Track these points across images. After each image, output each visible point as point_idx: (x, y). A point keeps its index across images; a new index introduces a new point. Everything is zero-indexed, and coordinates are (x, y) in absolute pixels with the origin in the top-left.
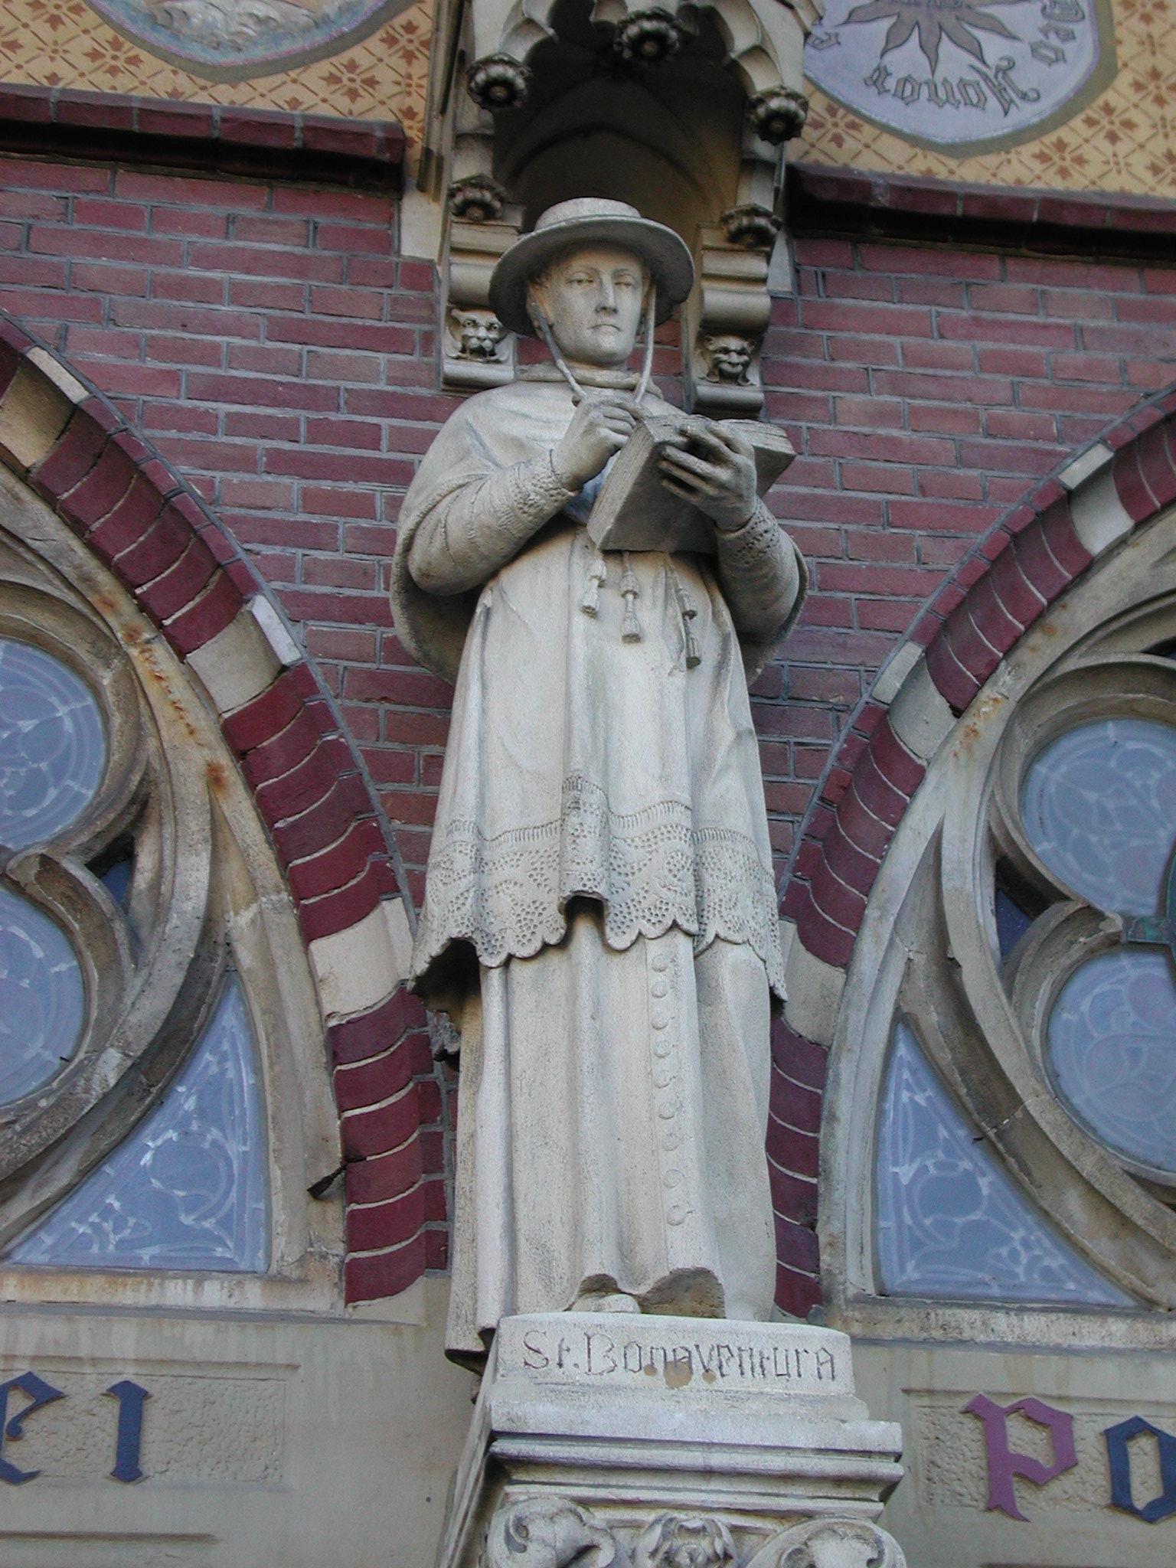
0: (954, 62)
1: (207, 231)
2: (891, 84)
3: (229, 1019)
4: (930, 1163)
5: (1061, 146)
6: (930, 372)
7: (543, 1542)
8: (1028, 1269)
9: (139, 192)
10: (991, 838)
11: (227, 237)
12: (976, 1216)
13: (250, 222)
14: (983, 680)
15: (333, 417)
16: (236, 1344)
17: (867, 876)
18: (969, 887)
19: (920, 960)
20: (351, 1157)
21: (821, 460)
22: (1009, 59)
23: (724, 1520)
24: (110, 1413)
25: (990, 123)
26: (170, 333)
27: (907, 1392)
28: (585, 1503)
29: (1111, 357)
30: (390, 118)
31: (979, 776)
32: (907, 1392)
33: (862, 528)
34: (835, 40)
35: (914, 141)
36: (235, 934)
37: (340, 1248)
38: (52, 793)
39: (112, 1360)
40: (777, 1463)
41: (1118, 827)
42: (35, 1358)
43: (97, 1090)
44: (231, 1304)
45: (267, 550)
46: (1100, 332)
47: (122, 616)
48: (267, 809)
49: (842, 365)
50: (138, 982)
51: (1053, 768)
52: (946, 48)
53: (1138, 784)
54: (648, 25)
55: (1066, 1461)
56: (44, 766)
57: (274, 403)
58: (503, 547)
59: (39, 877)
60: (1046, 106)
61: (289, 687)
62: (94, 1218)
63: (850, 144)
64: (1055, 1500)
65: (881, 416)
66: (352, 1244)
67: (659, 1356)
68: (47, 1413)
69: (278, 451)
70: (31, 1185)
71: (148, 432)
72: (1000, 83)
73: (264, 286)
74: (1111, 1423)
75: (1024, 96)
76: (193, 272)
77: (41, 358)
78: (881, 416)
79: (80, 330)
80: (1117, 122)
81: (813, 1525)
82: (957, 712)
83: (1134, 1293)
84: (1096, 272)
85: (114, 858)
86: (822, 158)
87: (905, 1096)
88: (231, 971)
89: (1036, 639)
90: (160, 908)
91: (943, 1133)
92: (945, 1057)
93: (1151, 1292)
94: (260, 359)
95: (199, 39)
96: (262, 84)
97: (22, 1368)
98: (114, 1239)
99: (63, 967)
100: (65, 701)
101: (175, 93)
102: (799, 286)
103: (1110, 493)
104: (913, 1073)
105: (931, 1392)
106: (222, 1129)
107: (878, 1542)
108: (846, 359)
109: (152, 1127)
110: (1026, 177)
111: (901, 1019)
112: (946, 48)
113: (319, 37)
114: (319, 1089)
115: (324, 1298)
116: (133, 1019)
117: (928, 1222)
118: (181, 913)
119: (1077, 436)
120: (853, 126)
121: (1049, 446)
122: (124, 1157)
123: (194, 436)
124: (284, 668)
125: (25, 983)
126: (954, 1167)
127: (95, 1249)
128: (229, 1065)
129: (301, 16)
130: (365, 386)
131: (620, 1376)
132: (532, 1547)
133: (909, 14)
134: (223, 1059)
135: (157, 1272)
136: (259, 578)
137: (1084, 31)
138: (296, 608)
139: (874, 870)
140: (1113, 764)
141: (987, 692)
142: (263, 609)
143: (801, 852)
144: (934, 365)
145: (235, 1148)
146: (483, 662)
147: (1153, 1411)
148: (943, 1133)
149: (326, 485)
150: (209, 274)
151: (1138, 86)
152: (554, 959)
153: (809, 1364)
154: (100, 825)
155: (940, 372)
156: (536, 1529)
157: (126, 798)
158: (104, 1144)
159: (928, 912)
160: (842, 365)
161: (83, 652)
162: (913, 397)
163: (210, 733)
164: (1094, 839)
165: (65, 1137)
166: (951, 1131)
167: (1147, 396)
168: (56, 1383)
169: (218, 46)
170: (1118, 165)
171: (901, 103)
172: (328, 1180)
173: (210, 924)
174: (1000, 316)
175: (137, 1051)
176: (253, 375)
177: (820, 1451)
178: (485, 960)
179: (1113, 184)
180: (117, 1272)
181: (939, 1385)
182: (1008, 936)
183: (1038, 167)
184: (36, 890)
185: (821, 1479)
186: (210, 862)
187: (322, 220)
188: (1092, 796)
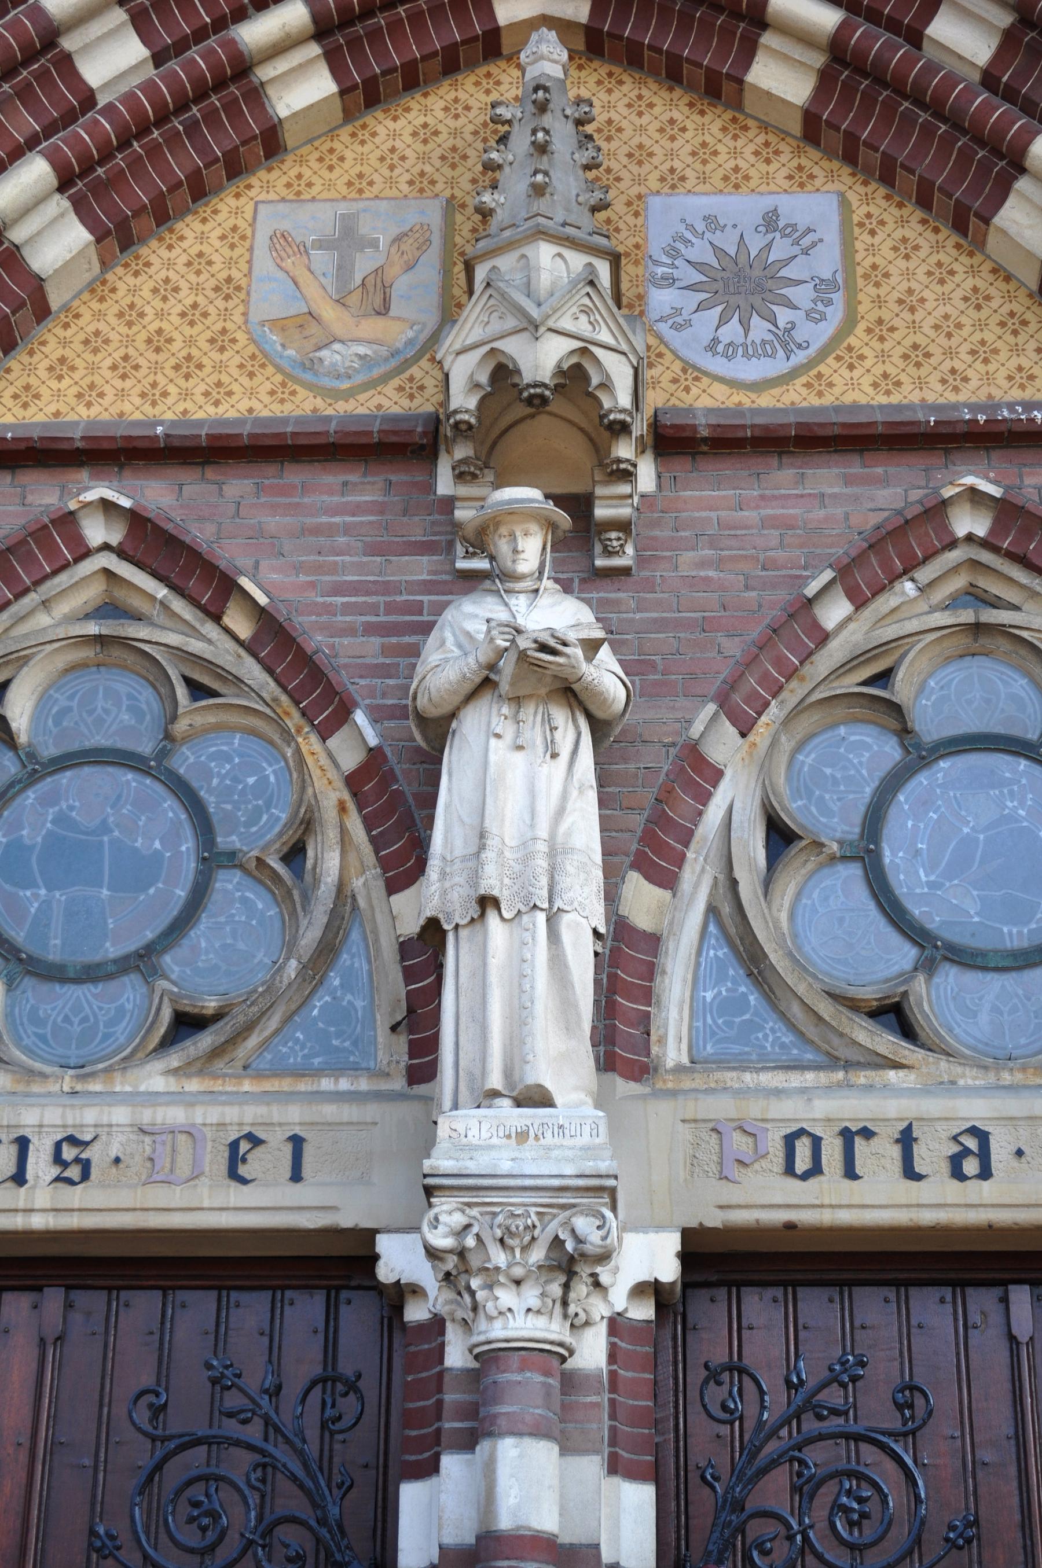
0: (759, 328)
1: (331, 493)
2: (720, 348)
3: (355, 935)
4: (723, 989)
5: (819, 376)
6: (732, 532)
7: (446, 1224)
8: (772, 1046)
9: (295, 475)
10: (764, 805)
11: (343, 495)
12: (747, 1017)
13: (355, 484)
14: (760, 714)
15: (398, 598)
16: (348, 1112)
17: (686, 837)
18: (746, 836)
19: (721, 877)
20: (411, 1011)
21: (666, 595)
22: (792, 323)
23: (533, 1210)
24: (288, 1149)
25: (777, 366)
26: (312, 558)
27: (683, 1121)
28: (469, 1205)
29: (839, 511)
30: (432, 409)
31: (755, 770)
32: (683, 1121)
33: (688, 636)
34: (689, 323)
35: (734, 384)
36: (356, 890)
37: (406, 1058)
38: (265, 817)
39: (289, 1124)
40: (556, 1182)
41: (842, 788)
42: (253, 1124)
43: (286, 982)
44: (352, 1088)
45: (363, 682)
46: (834, 496)
47: (294, 720)
48: (369, 824)
49: (683, 534)
50: (306, 922)
51: (807, 756)
52: (755, 319)
53: (855, 761)
54: (532, 391)
55: (761, 1156)
56: (260, 802)
57: (368, 593)
58: (457, 699)
59: (257, 867)
60: (812, 351)
61: (375, 755)
62: (290, 1044)
63: (694, 391)
64: (757, 1172)
65: (703, 564)
66: (411, 1056)
67: (513, 1130)
68: (259, 1151)
69: (368, 622)
70: (257, 1031)
71: (300, 619)
72: (786, 340)
73: (362, 523)
74: (789, 1131)
75: (799, 346)
76: (324, 519)
77: (245, 582)
78: (703, 564)
79: (264, 564)
80: (884, 328)
81: (574, 1210)
82: (743, 735)
83: (828, 1054)
84: (836, 457)
85: (295, 854)
86: (678, 403)
87: (712, 953)
88: (355, 907)
89: (794, 684)
90: (316, 882)
91: (731, 972)
92: (732, 931)
93: (836, 1053)
94: (360, 568)
95: (328, 374)
96: (362, 397)
97: (246, 1130)
98: (300, 1054)
99: (271, 913)
100: (270, 765)
101: (315, 410)
102: (659, 486)
103: (839, 590)
104: (717, 940)
105: (695, 1121)
106: (353, 994)
107: (603, 1217)
108: (684, 530)
109: (318, 995)
110: (797, 398)
111: (712, 910)
112: (755, 319)
113: (393, 363)
114: (395, 974)
115: (398, 1083)
116: (303, 943)
117: (720, 1021)
118: (326, 884)
119: (813, 566)
120: (696, 379)
121: (798, 572)
122: (304, 1012)
123: (324, 618)
124: (371, 749)
125: (254, 922)
126: (736, 990)
127: (292, 1060)
128: (356, 960)
129: (384, 351)
130: (416, 578)
131: (495, 1141)
132: (440, 1227)
133: (734, 300)
134: (353, 956)
135: (317, 1073)
136: (359, 699)
137: (838, 297)
138: (377, 716)
139: (691, 833)
140: (842, 750)
141: (764, 719)
142: (360, 717)
143: (643, 831)
144: (736, 528)
145: (359, 1004)
146: (450, 761)
147: (811, 1123)
148: (731, 972)
149: (394, 640)
150: (333, 520)
151: (869, 331)
152: (478, 926)
153: (586, 1129)
154: (285, 838)
155: (739, 532)
156: (443, 1218)
157: (298, 821)
158: (293, 1007)
159: (725, 852)
160: (683, 534)
161: (276, 738)
162: (722, 550)
163: (339, 784)
164: (827, 796)
165: (271, 1006)
166: (735, 971)
167: (860, 533)
168: (262, 1135)
169: (338, 377)
170: (853, 385)
171: (725, 360)
172: (399, 1024)
173: (341, 887)
174: (776, 492)
175: (305, 960)
176: (356, 578)
177: (578, 1176)
178: (446, 927)
179: (848, 399)
180: (299, 1073)
181: (699, 1117)
182: (773, 857)
183: (804, 391)
184: (256, 873)
185: (578, 1189)
186: (341, 855)
187: (394, 478)
188: (828, 771)
